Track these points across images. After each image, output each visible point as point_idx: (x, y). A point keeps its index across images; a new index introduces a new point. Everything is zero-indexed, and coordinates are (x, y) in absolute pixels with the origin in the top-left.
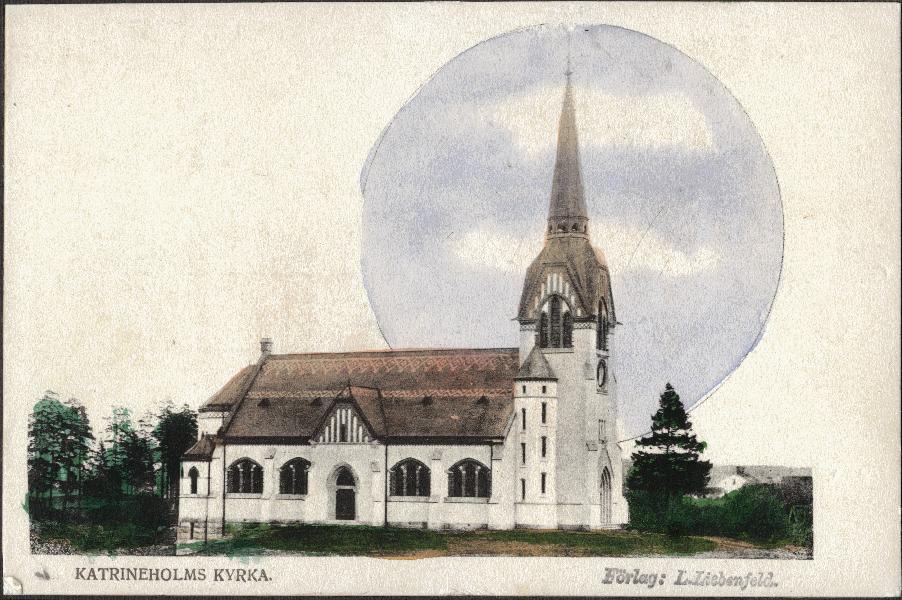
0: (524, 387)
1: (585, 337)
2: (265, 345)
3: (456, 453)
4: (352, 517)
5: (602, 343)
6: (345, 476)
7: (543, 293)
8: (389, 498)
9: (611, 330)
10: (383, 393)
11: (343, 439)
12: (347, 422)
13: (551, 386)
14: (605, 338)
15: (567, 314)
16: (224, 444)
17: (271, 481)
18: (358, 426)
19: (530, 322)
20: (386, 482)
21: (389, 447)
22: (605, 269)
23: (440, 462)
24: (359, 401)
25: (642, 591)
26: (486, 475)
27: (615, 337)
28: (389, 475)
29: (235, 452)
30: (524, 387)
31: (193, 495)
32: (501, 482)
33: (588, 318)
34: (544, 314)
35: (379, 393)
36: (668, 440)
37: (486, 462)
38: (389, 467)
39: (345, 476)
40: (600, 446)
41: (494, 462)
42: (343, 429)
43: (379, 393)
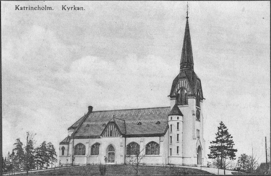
0: (171, 117)
1: (192, 101)
2: (90, 108)
3: (148, 140)
4: (113, 161)
5: (198, 104)
6: (111, 147)
7: (178, 87)
8: (126, 155)
9: (201, 100)
10: (126, 122)
11: (111, 135)
12: (112, 130)
13: (180, 117)
14: (199, 103)
15: (186, 94)
16: (74, 139)
17: (88, 150)
18: (116, 131)
19: (174, 97)
20: (125, 151)
21: (127, 138)
22: (193, 64)
23: (143, 143)
24: (117, 123)
25: (22, 4)
26: (158, 145)
27: (204, 105)
28: (126, 148)
29: (77, 141)
30: (171, 117)
31: (63, 156)
32: (163, 149)
33: (192, 95)
34: (179, 94)
35: (125, 122)
36: (222, 141)
37: (158, 142)
38: (127, 145)
39: (111, 147)
40: (197, 139)
41: (161, 142)
42: (111, 132)
43: (125, 122)
